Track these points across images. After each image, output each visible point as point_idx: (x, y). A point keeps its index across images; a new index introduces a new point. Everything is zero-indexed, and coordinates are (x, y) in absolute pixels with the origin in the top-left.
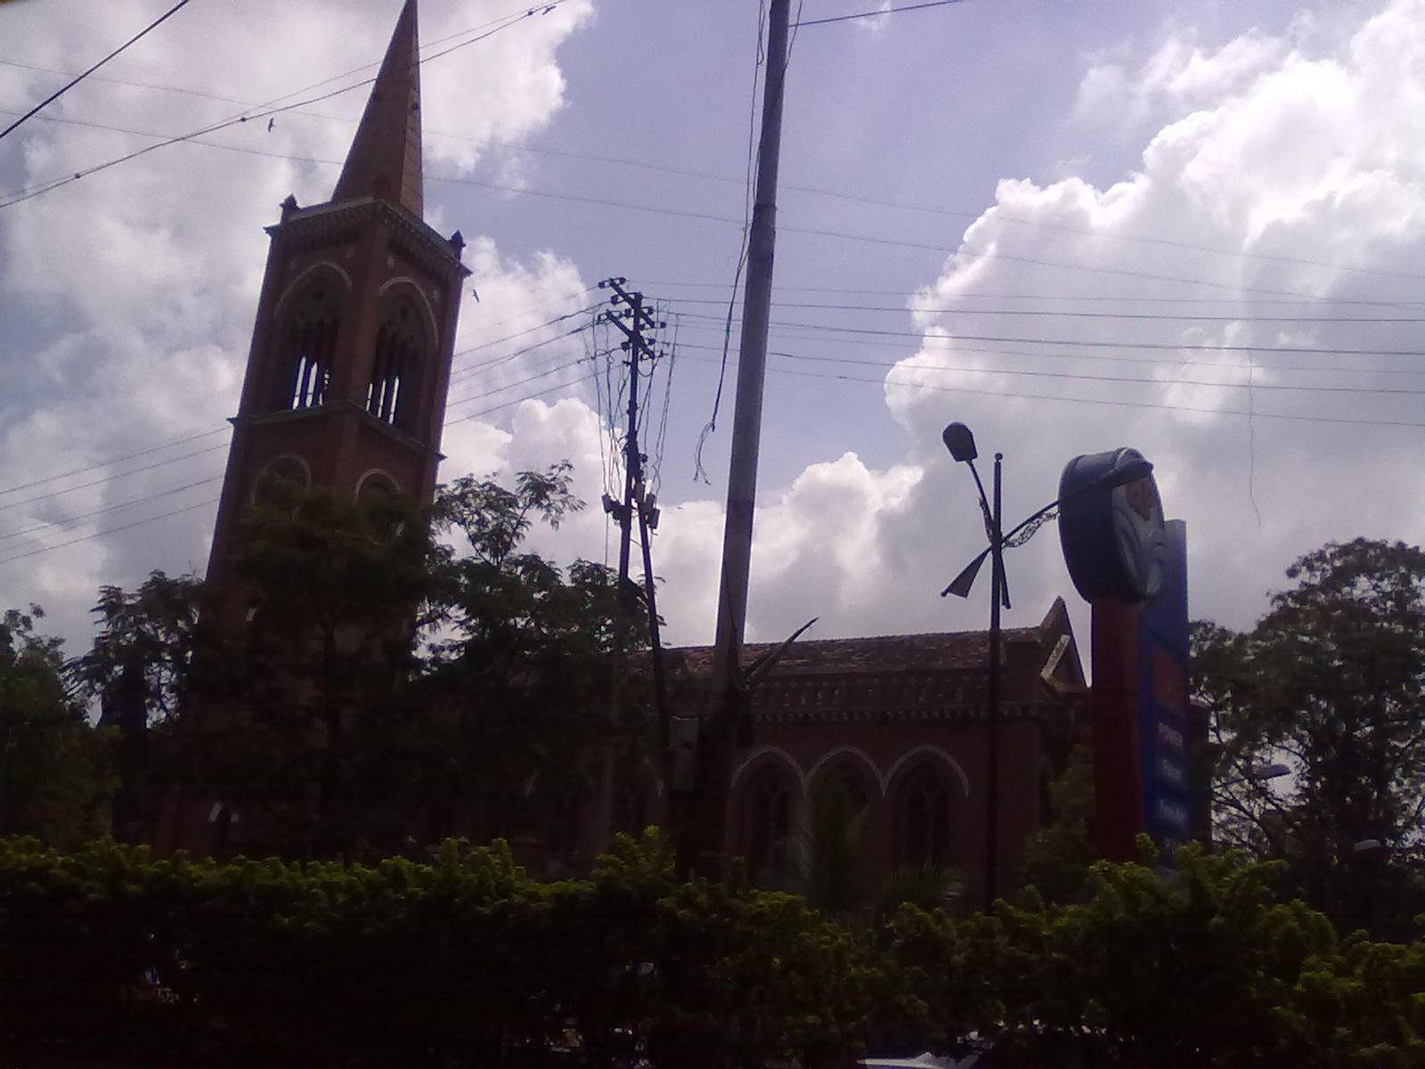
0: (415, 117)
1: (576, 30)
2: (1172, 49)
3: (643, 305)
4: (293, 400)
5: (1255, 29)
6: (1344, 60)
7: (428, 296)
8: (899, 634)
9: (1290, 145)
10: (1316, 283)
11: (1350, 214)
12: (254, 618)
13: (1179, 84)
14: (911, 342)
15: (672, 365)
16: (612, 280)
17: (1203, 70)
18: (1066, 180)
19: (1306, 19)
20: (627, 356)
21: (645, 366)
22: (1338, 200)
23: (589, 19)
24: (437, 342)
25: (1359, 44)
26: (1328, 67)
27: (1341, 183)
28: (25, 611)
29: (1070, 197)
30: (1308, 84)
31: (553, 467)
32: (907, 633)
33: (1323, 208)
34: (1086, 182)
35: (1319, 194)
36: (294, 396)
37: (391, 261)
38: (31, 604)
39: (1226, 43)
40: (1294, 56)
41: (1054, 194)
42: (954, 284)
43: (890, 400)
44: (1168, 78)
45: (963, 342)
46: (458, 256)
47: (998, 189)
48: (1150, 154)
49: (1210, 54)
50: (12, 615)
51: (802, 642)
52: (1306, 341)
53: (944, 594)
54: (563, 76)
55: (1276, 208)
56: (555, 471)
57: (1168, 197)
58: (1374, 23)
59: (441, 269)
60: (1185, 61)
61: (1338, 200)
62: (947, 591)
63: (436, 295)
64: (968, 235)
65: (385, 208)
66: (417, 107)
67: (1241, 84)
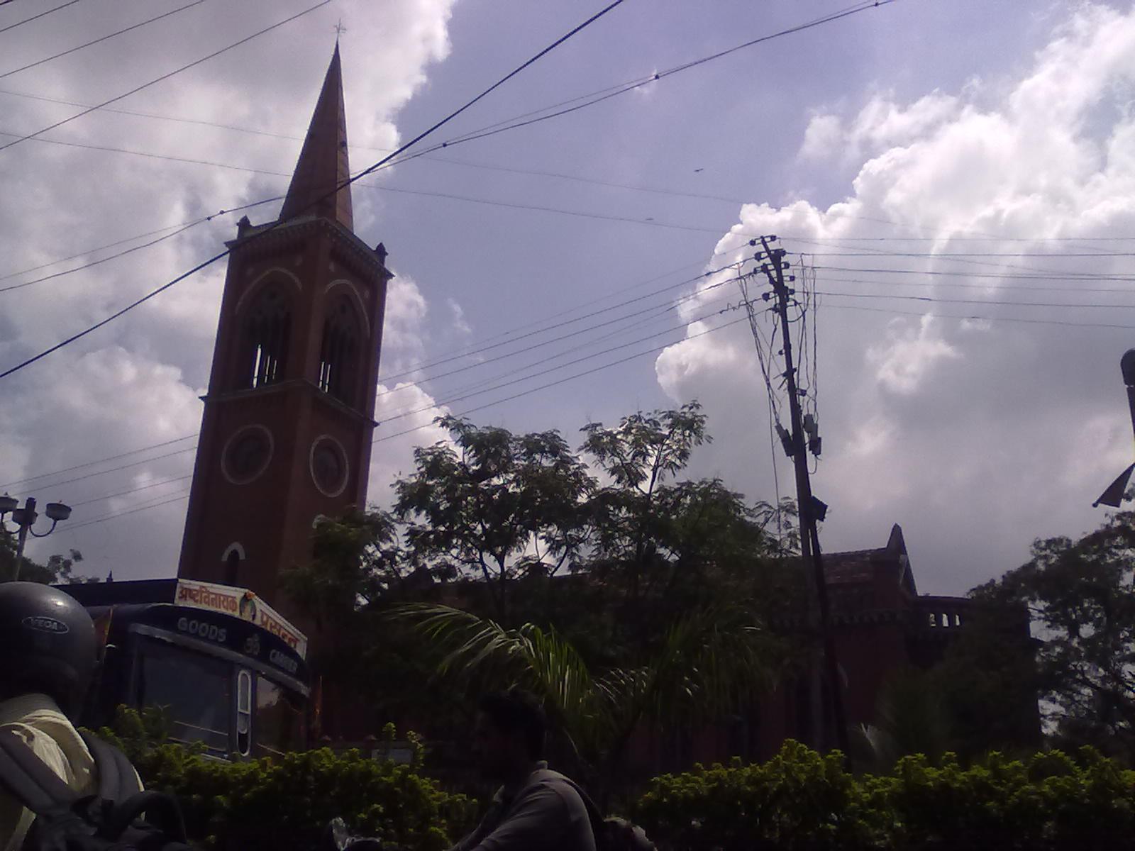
0: (344, 153)
1: (414, 96)
2: (875, 107)
3: (782, 261)
4: (253, 381)
5: (937, 90)
6: (1007, 113)
7: (361, 296)
8: (833, 552)
9: (968, 176)
10: (987, 285)
11: (1003, 230)
12: (228, 559)
13: (881, 132)
14: (678, 333)
15: (815, 310)
16: (763, 238)
17: (898, 121)
18: (795, 203)
19: (976, 82)
20: (774, 300)
21: (792, 312)
22: (1005, 215)
23: (424, 87)
24: (369, 331)
25: (1016, 99)
26: (995, 118)
27: (1007, 204)
28: (67, 556)
29: (800, 216)
30: (977, 130)
31: (684, 407)
32: (839, 551)
33: (993, 221)
34: (812, 205)
35: (988, 212)
36: (258, 377)
37: (332, 267)
38: (71, 550)
39: (915, 101)
40: (968, 109)
41: (786, 215)
42: (706, 291)
43: (661, 380)
44: (872, 128)
45: (716, 335)
46: (383, 262)
47: (742, 212)
48: (858, 182)
49: (903, 109)
50: (55, 559)
51: (560, 577)
52: (983, 326)
53: (1095, 505)
54: (398, 131)
55: (955, 224)
56: (686, 410)
57: (875, 218)
58: (1027, 84)
59: (368, 271)
60: (884, 113)
61: (1005, 215)
62: (1099, 501)
63: (367, 294)
64: (720, 247)
65: (327, 224)
66: (344, 144)
67: (928, 132)
